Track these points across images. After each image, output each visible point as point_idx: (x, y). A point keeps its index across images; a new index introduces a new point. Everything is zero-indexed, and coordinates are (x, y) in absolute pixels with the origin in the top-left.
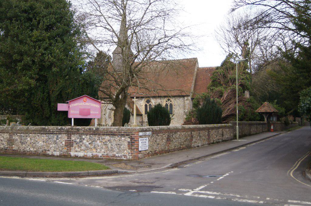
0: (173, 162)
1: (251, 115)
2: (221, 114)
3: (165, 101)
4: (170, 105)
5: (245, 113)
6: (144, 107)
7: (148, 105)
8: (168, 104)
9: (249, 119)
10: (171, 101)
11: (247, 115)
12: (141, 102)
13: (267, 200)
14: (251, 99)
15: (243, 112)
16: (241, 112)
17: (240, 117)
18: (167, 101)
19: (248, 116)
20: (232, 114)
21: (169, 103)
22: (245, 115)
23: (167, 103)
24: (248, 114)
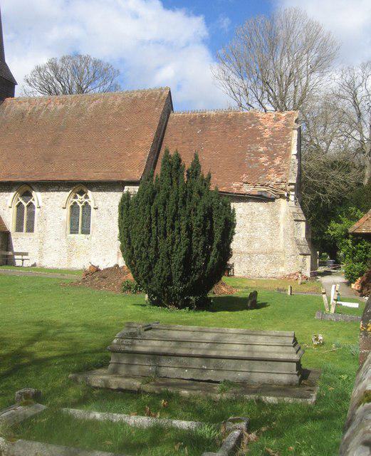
4: (83, 207)
7: (25, 205)
8: (79, 204)
23: (75, 200)
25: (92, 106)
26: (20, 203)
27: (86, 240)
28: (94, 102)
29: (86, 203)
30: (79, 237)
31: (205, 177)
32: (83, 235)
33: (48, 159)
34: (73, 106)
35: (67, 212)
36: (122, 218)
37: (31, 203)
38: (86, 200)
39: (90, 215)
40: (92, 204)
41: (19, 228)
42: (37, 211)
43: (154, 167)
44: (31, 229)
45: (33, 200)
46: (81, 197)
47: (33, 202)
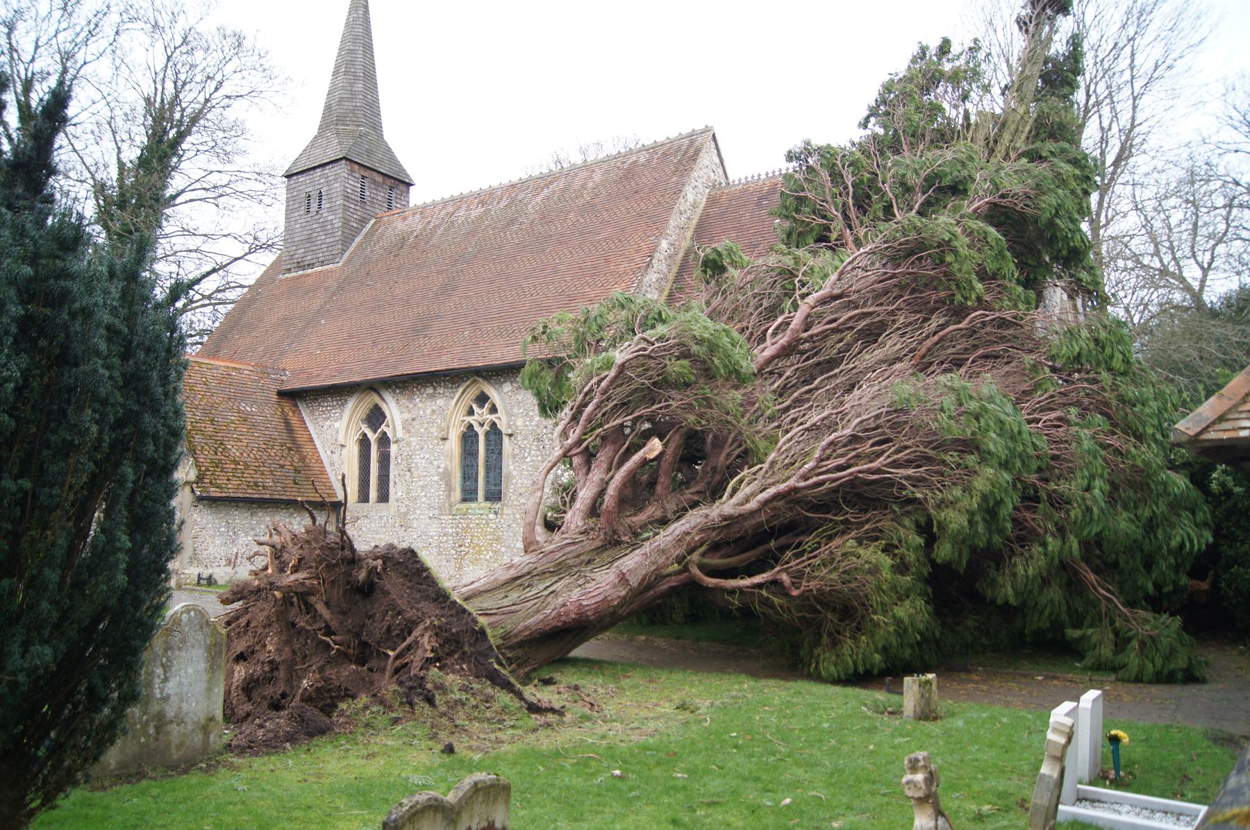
0: (880, 710)
1: (1112, 497)
2: (1184, 622)
3: (463, 409)
4: (487, 434)
5: (1033, 478)
6: (353, 450)
7: (372, 437)
8: (477, 428)
9: (1085, 545)
10: (494, 410)
11: (1059, 502)
12: (337, 425)
13: (1051, 259)
14: (1097, 341)
15: (1005, 465)
16: (971, 459)
17: (1122, 599)
18: (471, 412)
19: (1075, 513)
20: (854, 482)
21: (482, 425)
22: (1030, 499)
23: (470, 419)
24: (1070, 488)
25: (539, 199)
26: (365, 435)
27: (492, 516)
28: (546, 191)
29: (493, 425)
30: (480, 505)
31: (169, 192)
32: (488, 504)
33: (420, 328)
34: (502, 205)
35: (454, 445)
36: (551, 526)
37: (384, 434)
38: (493, 417)
39: (500, 453)
40: (502, 426)
41: (364, 497)
42: (394, 449)
43: (761, 492)
44: (384, 497)
45: (388, 426)
46: (480, 411)
47: (386, 429)
